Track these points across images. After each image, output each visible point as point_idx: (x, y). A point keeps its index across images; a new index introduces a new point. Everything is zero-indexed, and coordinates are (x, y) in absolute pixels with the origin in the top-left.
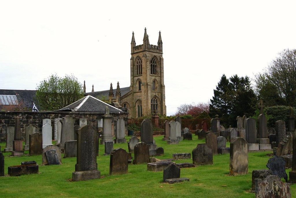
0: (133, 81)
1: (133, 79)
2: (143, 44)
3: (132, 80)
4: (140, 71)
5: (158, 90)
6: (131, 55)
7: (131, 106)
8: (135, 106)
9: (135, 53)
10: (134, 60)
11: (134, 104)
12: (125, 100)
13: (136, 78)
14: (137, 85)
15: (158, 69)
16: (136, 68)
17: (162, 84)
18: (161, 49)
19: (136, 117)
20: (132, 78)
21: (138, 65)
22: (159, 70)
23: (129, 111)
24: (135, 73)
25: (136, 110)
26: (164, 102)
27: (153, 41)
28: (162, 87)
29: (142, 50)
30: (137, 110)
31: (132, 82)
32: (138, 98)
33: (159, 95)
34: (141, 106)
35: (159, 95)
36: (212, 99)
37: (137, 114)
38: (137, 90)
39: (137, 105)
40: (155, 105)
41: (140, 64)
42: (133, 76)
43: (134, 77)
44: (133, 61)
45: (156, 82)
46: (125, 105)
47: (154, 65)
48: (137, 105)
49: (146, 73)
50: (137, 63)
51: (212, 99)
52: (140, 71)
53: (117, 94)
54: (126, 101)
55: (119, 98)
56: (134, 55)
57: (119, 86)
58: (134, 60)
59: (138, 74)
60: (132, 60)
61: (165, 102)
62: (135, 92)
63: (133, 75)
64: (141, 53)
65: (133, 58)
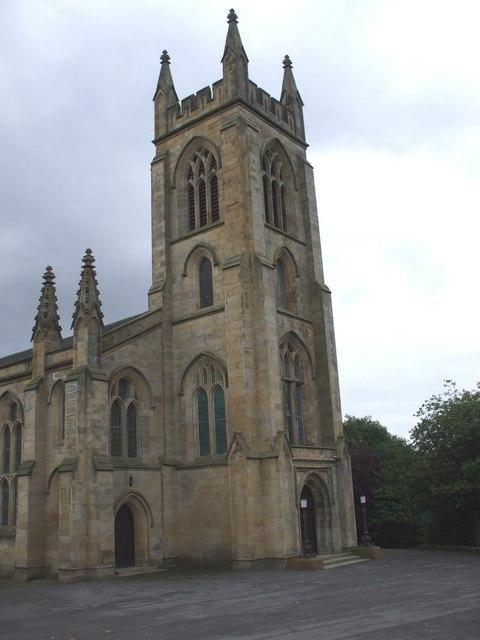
0: (168, 264)
1: (168, 252)
2: (220, 76)
3: (163, 258)
4: (208, 208)
5: (300, 305)
6: (153, 148)
7: (157, 392)
8: (176, 392)
9: (176, 132)
10: (173, 165)
11: (171, 386)
12: (122, 356)
13: (186, 246)
14: (192, 282)
15: (294, 209)
16: (188, 191)
17: (317, 279)
18: (299, 125)
19: (184, 452)
20: (162, 247)
21: (194, 183)
22: (299, 215)
23: (147, 418)
24: (179, 222)
25: (188, 413)
26: (332, 373)
27: (266, 77)
28: (319, 295)
29: (214, 106)
30: (192, 413)
31: (163, 269)
32: (200, 347)
33: (306, 335)
34: (218, 390)
35: (306, 335)
36: (53, 281)
37: (194, 434)
38: (192, 305)
39: (190, 388)
40: (293, 385)
41: (205, 177)
42: (166, 237)
43: (170, 243)
44: (167, 167)
45: (290, 268)
46: (124, 383)
47: (274, 183)
48: (190, 388)
49: (246, 206)
50: (190, 175)
51: (53, 281)
52: (208, 208)
53: (81, 314)
54: (127, 361)
55: (94, 338)
56: (170, 142)
57: (94, 274)
58: (173, 165)
59: (192, 225)
60: (161, 165)
61: (336, 370)
62: (176, 317)
63: (168, 233)
64: (209, 122)
65: (167, 154)
